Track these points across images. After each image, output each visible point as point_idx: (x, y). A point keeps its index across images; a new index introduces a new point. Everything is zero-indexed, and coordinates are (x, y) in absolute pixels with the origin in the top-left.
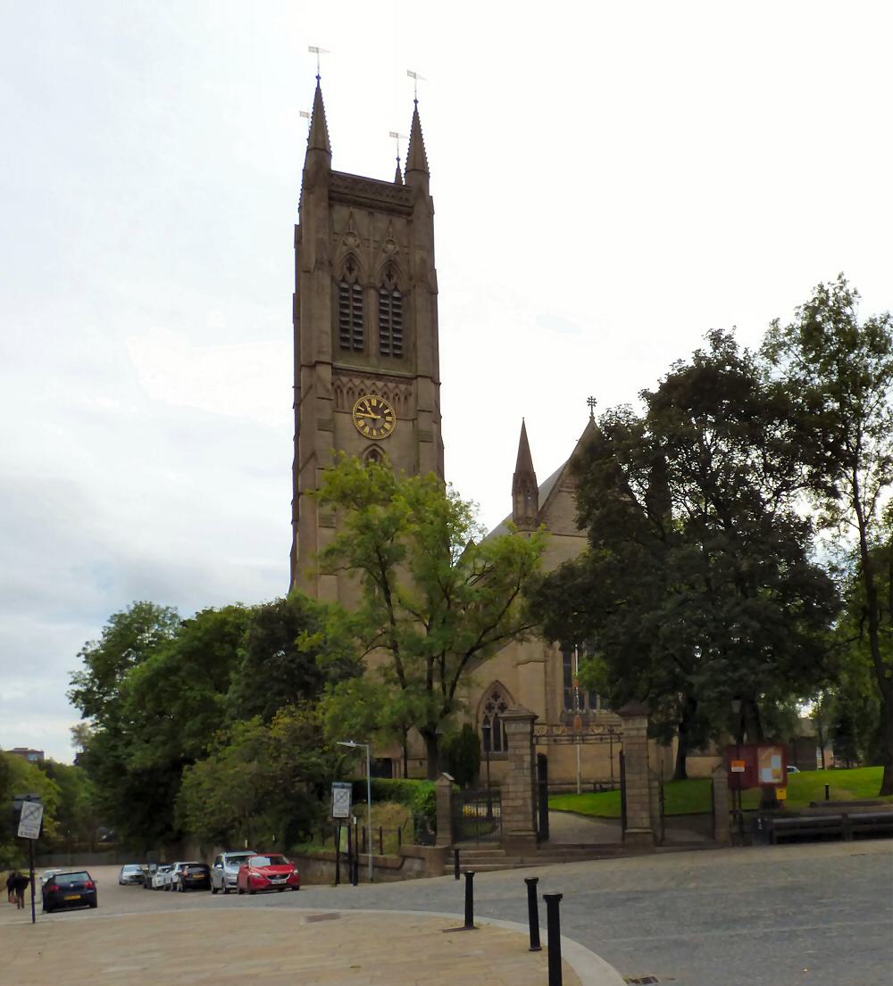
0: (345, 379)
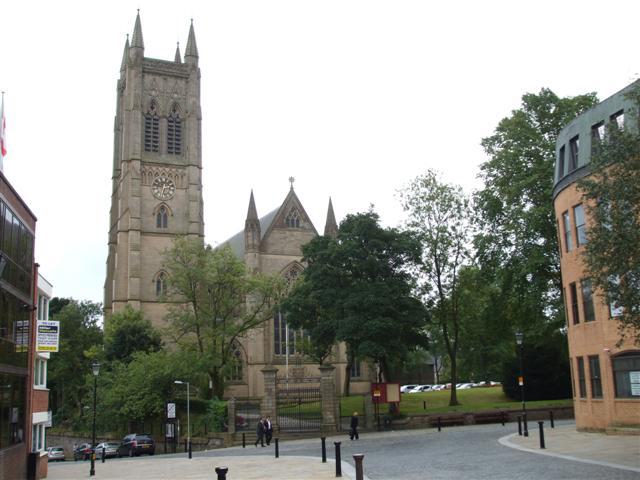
0: (147, 167)
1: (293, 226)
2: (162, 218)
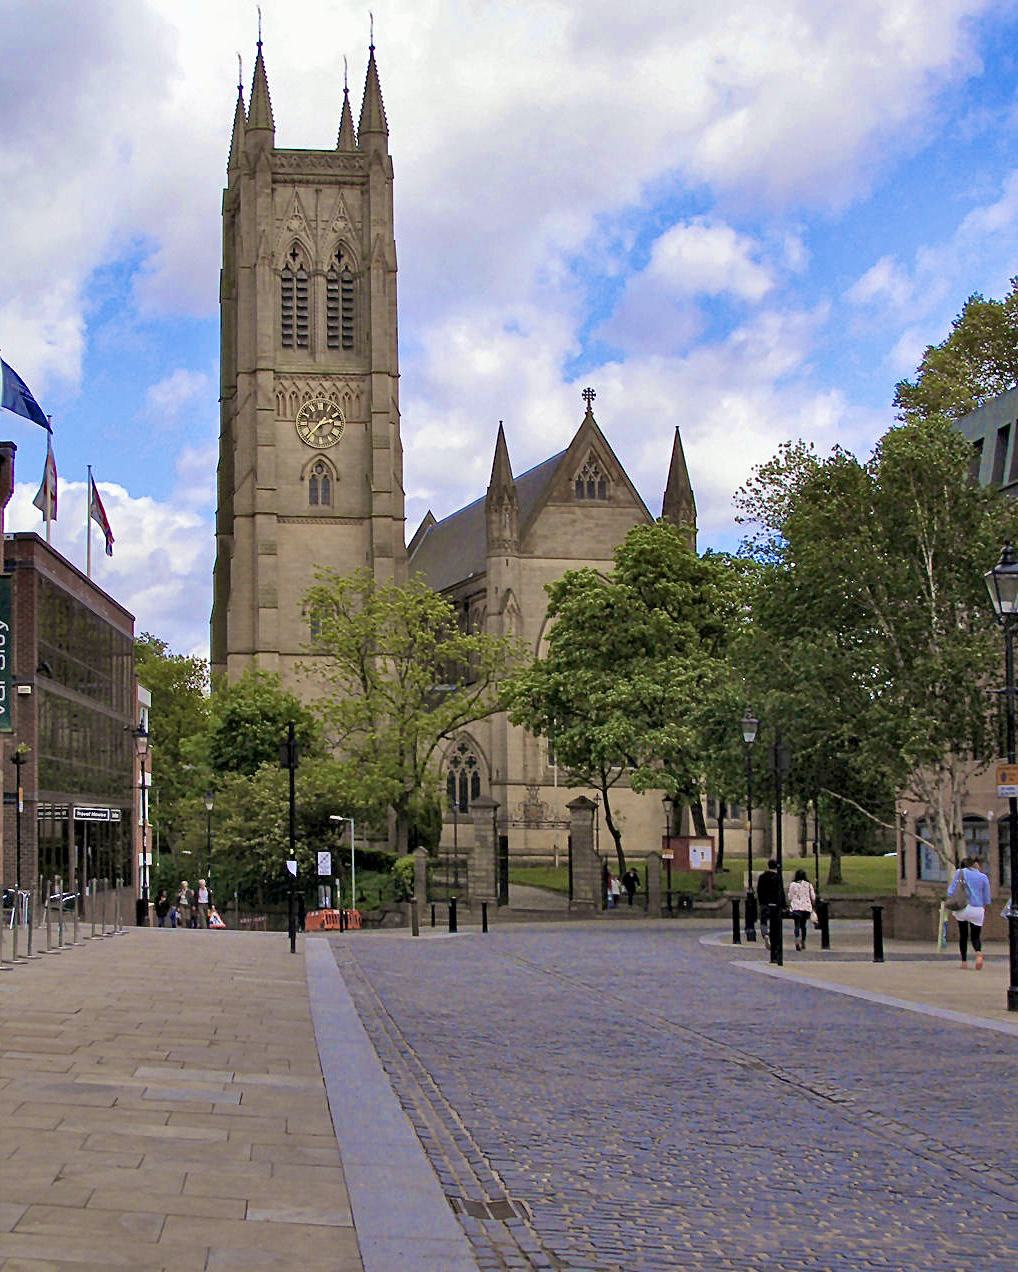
0: (286, 383)
1: (592, 496)
2: (320, 486)
